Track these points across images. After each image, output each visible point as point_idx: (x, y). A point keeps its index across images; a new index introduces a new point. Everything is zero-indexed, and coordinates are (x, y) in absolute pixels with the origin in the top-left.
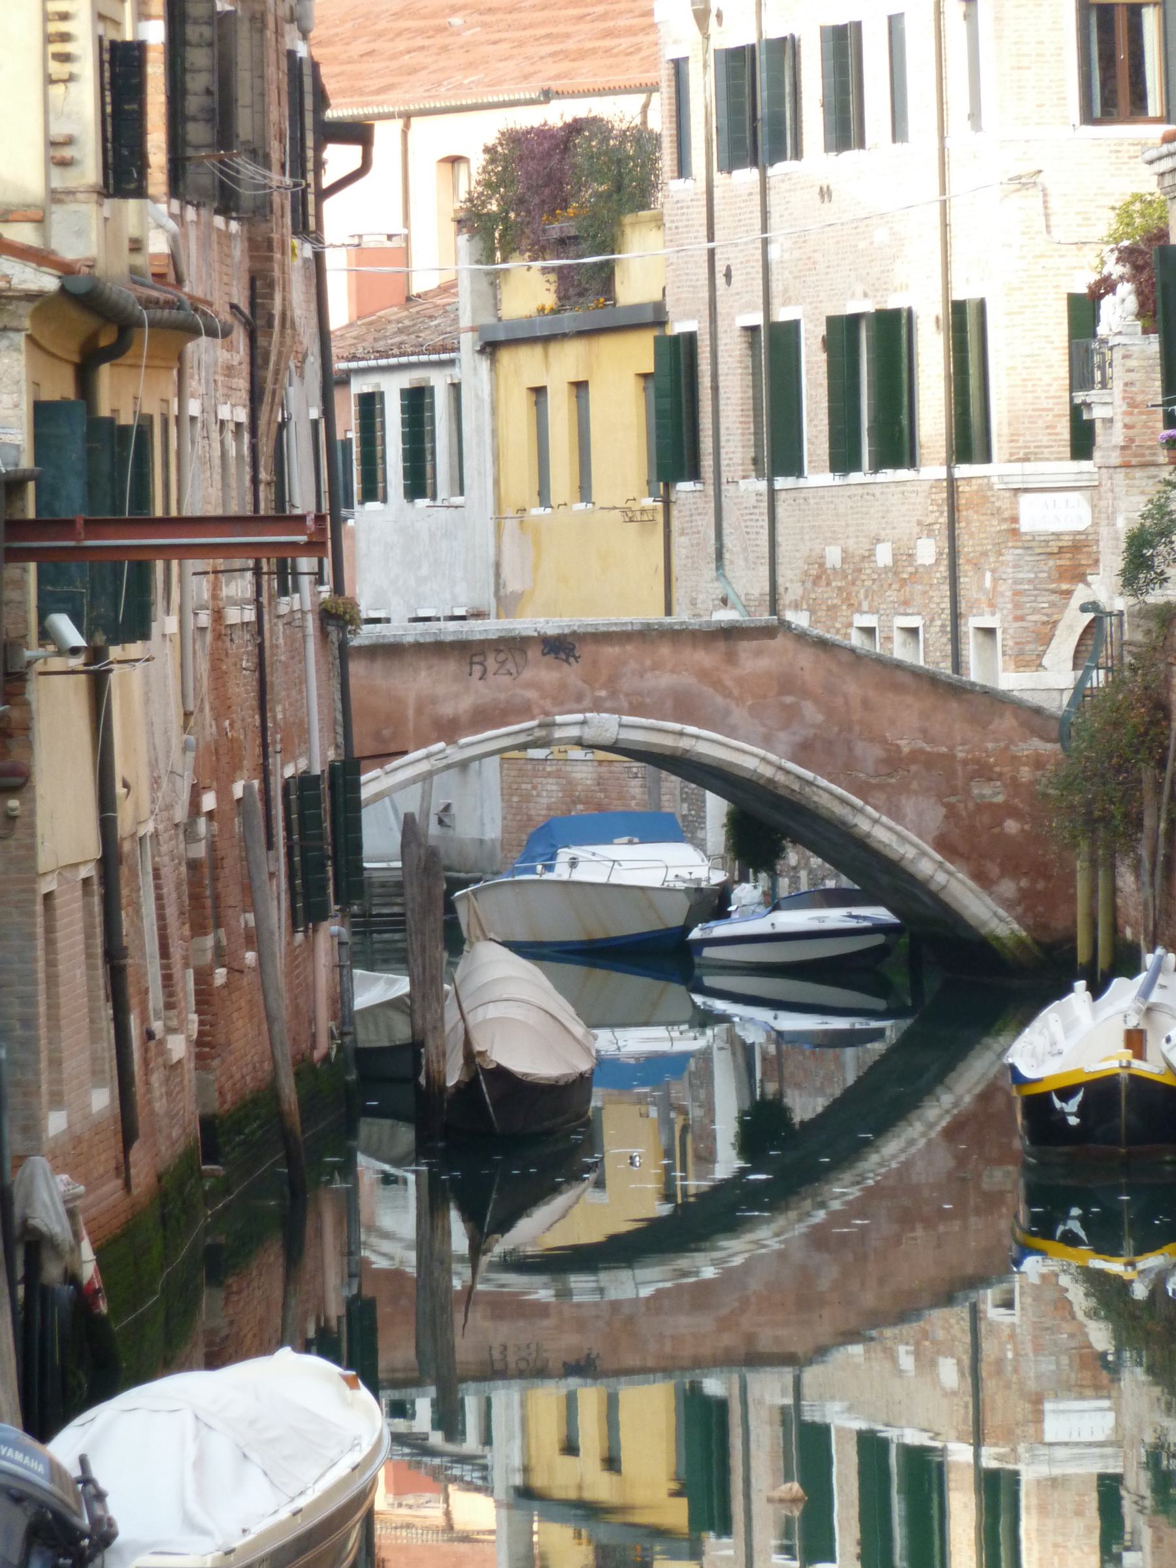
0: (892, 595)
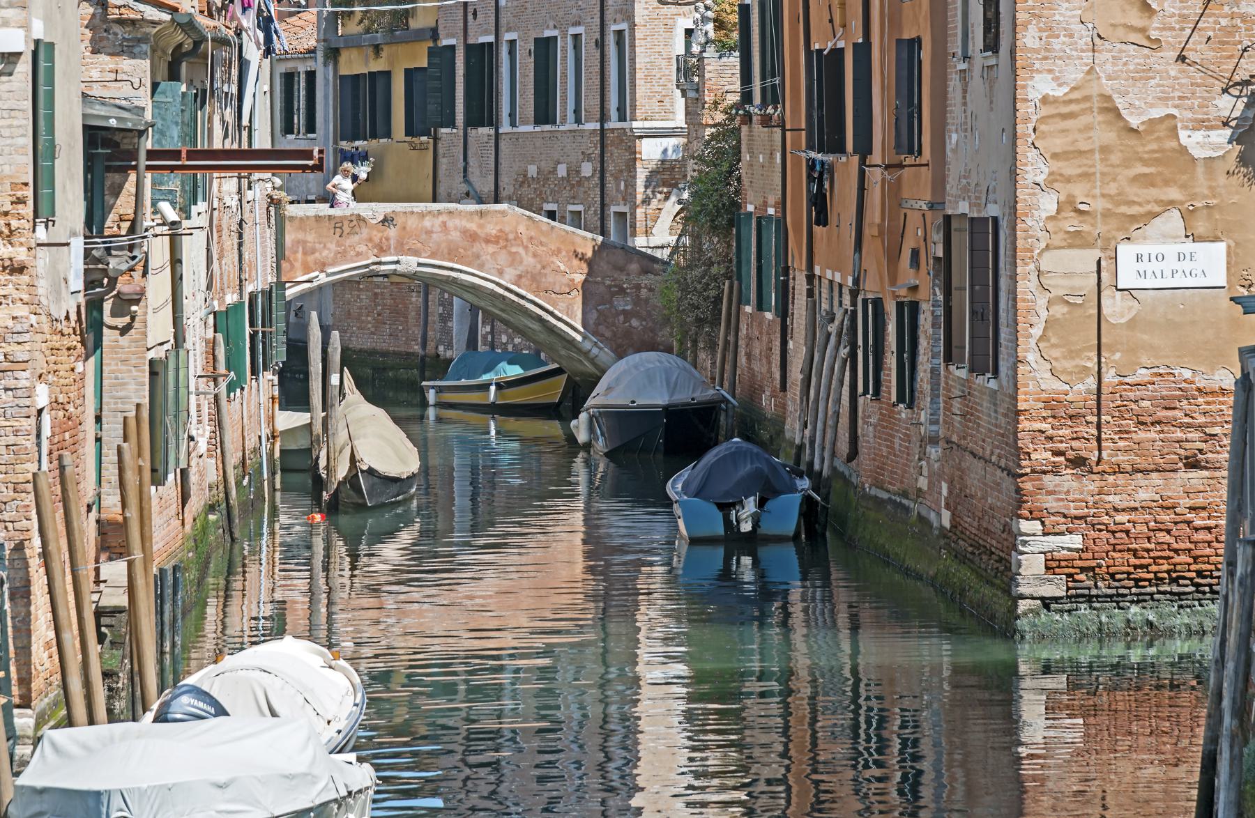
0: (566, 193)
